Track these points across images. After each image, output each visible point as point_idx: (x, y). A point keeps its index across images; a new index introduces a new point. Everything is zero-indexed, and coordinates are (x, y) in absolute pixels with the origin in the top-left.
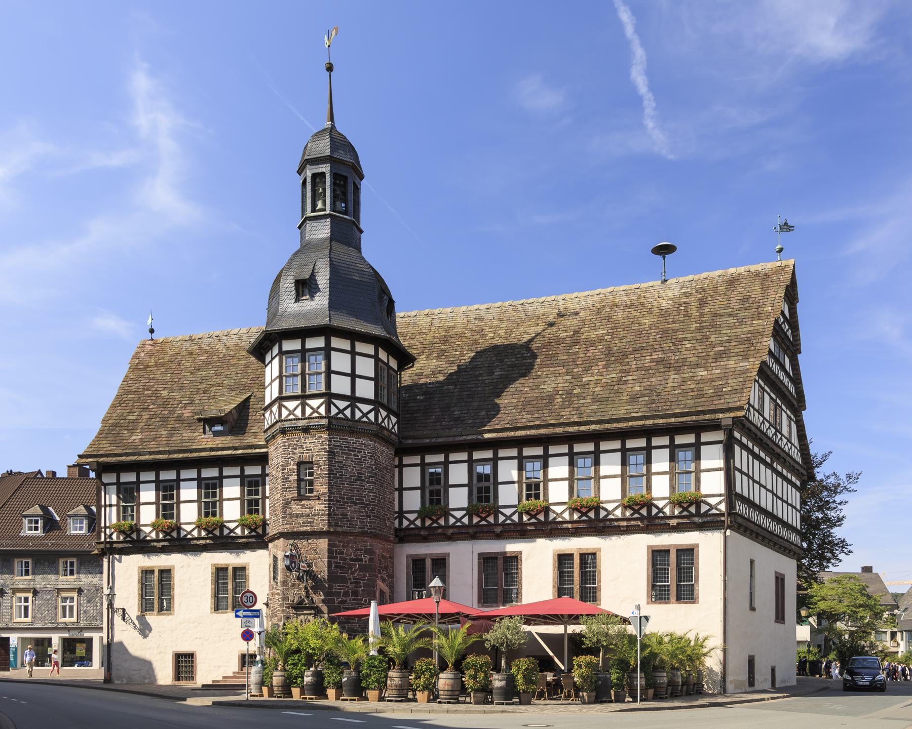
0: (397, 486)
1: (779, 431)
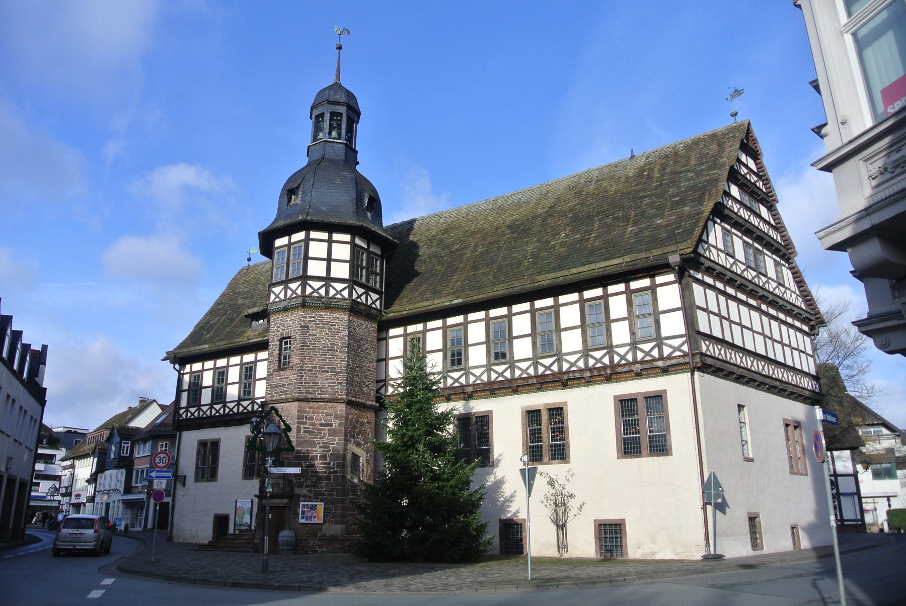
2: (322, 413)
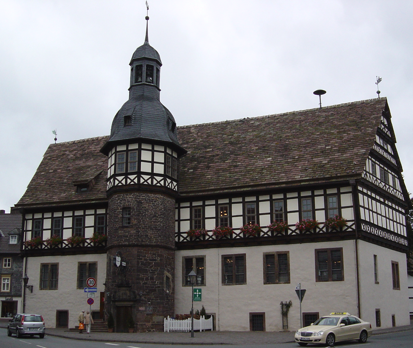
0: (177, 219)
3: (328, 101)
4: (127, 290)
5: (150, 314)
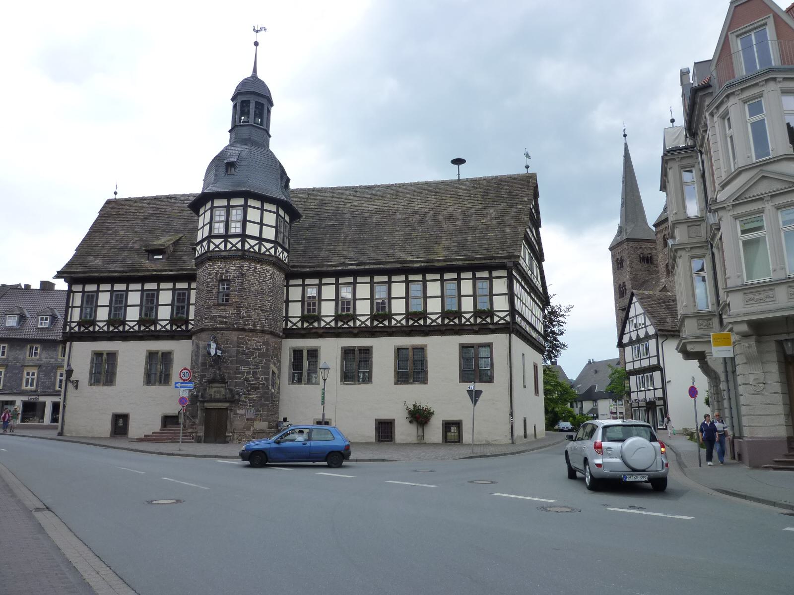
1: (533, 273)
2: (254, 340)
3: (467, 172)
4: (222, 387)
5: (251, 419)
